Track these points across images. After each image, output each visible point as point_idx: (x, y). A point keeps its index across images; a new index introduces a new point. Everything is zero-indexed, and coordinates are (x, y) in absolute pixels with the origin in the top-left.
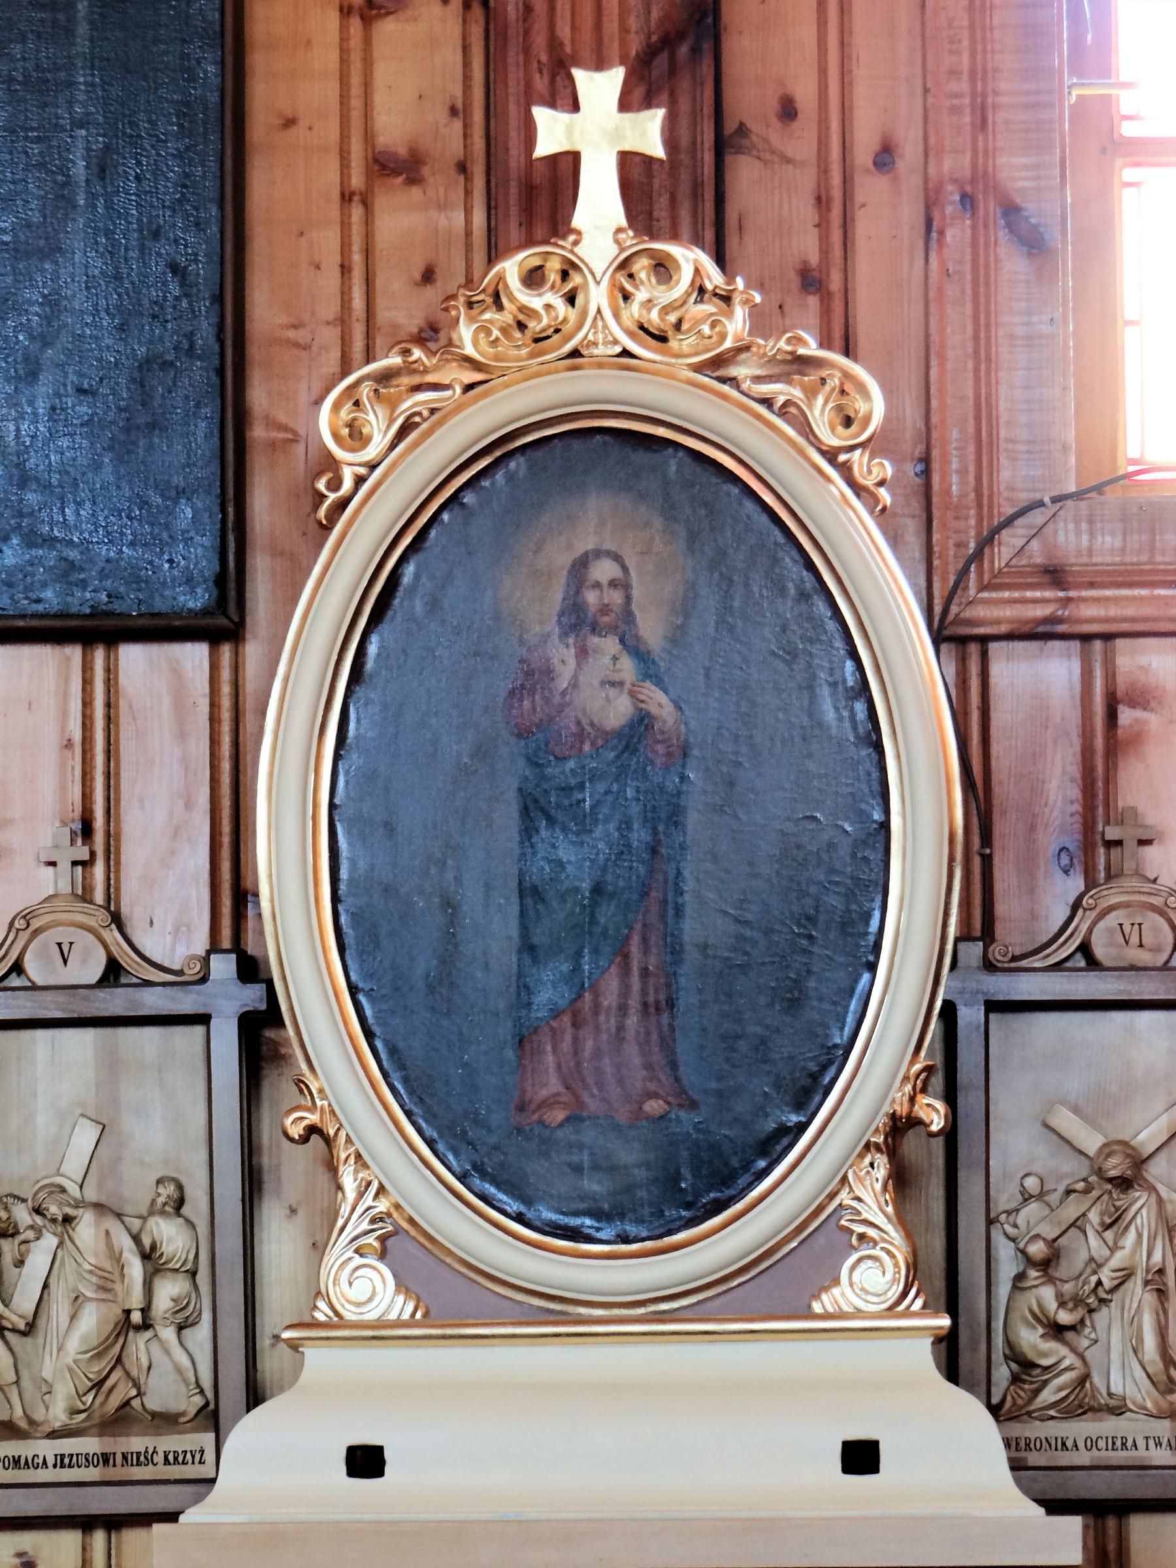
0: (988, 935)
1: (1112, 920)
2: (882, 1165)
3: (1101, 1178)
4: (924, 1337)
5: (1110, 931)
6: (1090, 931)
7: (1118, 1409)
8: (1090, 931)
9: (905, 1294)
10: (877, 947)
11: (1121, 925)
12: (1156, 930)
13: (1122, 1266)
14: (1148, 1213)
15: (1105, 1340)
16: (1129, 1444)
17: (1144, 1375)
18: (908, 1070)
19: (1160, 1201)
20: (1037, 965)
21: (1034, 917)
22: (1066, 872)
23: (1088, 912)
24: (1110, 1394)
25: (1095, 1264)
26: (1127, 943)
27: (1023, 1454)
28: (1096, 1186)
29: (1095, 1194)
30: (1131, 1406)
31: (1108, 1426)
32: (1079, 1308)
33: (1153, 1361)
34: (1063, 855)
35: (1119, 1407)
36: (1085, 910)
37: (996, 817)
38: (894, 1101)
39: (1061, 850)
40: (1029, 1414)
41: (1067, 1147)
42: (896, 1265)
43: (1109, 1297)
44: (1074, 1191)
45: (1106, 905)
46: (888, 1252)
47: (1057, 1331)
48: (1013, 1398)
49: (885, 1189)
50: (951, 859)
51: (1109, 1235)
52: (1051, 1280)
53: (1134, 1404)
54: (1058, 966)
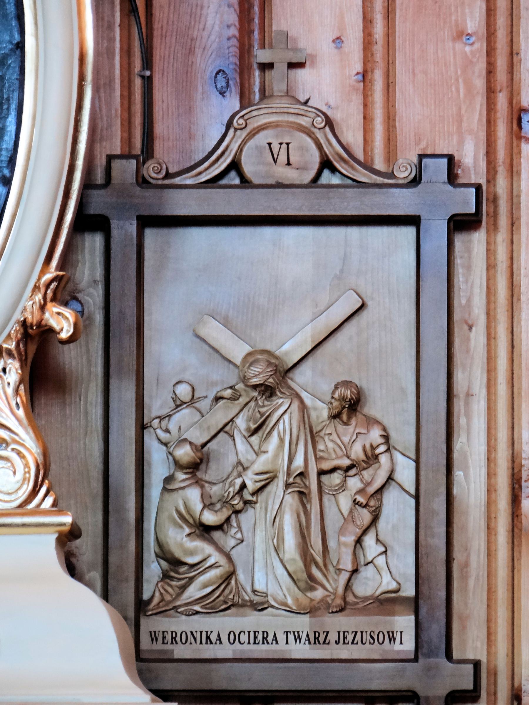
0: (148, 151)
1: (262, 139)
2: (13, 370)
3: (247, 386)
4: (48, 533)
5: (259, 148)
6: (240, 149)
7: (260, 607)
8: (240, 149)
9: (34, 492)
10: (12, 162)
11: (270, 144)
12: (302, 149)
13: (265, 469)
14: (290, 420)
15: (251, 540)
16: (270, 638)
17: (286, 573)
18: (39, 278)
19: (303, 407)
20: (189, 182)
21: (191, 137)
22: (222, 94)
23: (239, 132)
24: (254, 591)
25: (242, 467)
26: (275, 161)
27: (169, 647)
28: (243, 393)
29: (242, 400)
30: (273, 603)
31: (251, 621)
32: (224, 510)
33: (293, 560)
34: (220, 76)
35: (263, 603)
36: (236, 130)
37: (157, 41)
38: (25, 309)
39: (218, 73)
40: (175, 608)
41: (216, 355)
42: (26, 465)
43: (254, 499)
44: (222, 398)
45: (256, 125)
46: (19, 453)
47: (204, 531)
48: (161, 594)
49: (17, 391)
50: (82, 78)
51: (255, 440)
52: (199, 483)
53: (275, 600)
54: (213, 182)
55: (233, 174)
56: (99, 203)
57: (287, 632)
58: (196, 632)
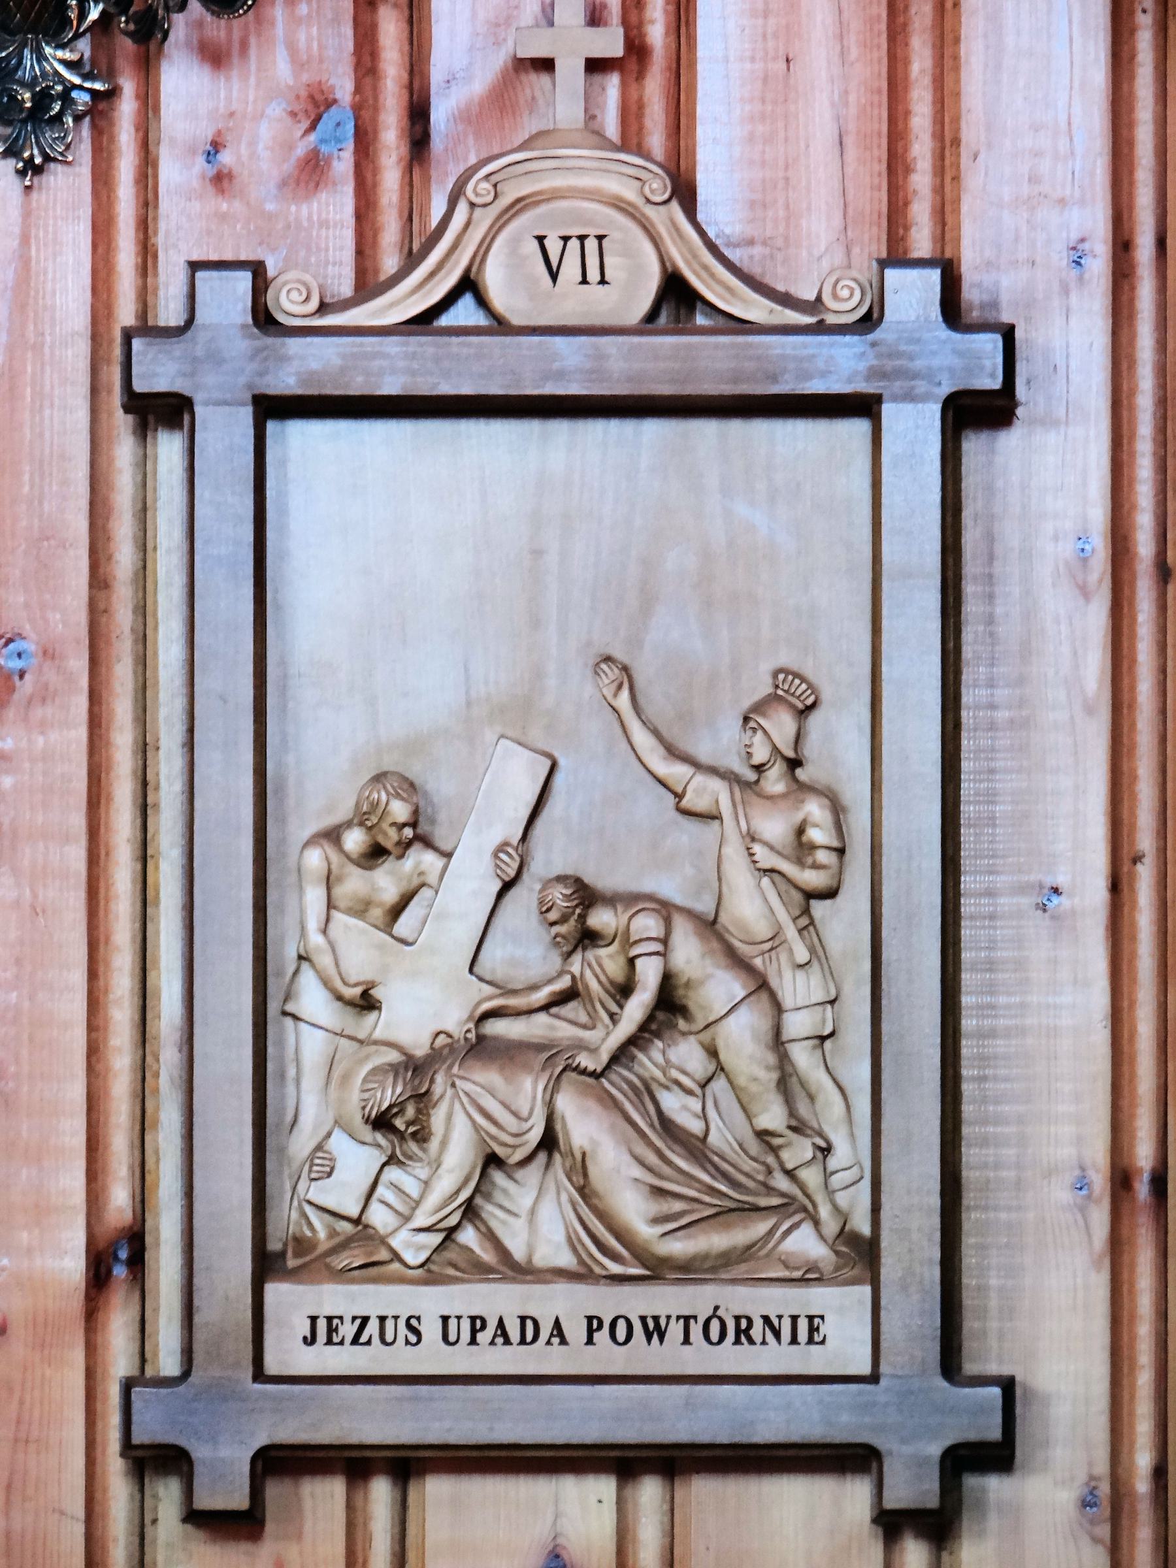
23: (478, 212)
26: (554, 276)
36: (472, 205)
54: (424, 321)
55: (467, 300)
56: (157, 372)
57: (687, 1319)
58: (780, 1317)
